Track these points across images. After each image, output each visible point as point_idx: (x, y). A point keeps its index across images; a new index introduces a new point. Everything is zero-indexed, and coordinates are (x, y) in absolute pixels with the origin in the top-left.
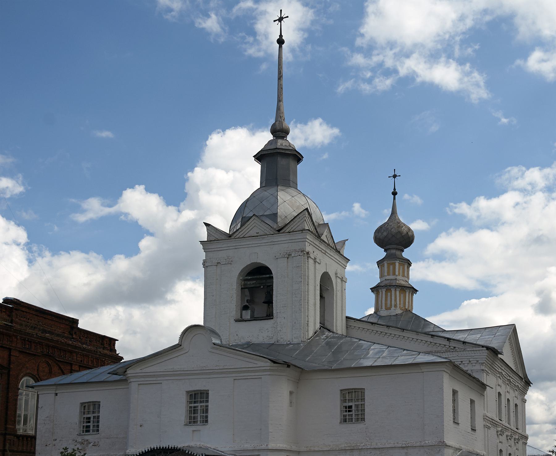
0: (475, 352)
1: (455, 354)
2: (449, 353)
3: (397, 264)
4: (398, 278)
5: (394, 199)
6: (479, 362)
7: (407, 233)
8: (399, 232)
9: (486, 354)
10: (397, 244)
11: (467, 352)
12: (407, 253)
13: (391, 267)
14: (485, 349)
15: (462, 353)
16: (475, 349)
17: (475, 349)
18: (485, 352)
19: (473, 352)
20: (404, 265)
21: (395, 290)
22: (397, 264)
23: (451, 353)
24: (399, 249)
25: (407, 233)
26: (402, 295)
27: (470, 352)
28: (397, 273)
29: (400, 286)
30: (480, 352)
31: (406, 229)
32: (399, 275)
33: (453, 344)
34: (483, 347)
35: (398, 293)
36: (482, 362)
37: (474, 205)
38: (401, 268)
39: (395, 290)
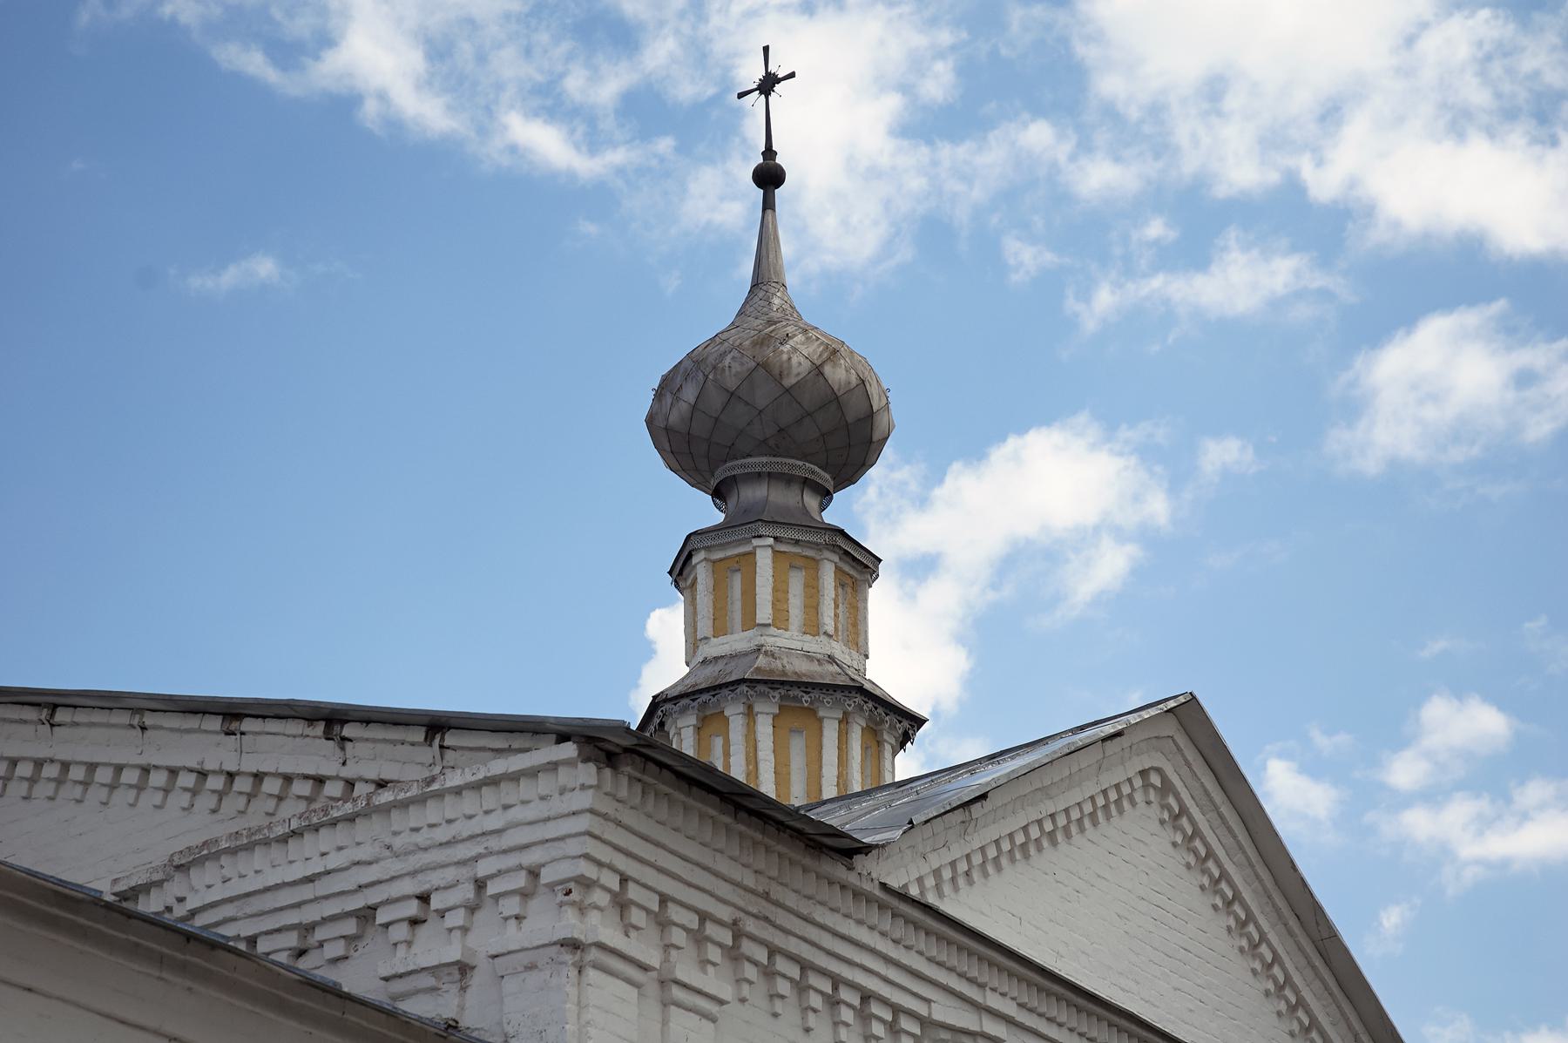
0: (508, 793)
1: (366, 838)
2: (326, 839)
3: (764, 560)
4: (778, 640)
5: (768, 204)
6: (547, 876)
7: (818, 370)
8: (764, 366)
9: (584, 800)
10: (764, 447)
11: (450, 807)
12: (859, 509)
13: (737, 582)
14: (569, 750)
15: (415, 817)
16: (499, 766)
17: (499, 766)
18: (579, 784)
19: (489, 797)
20: (813, 565)
21: (750, 714)
22: (764, 560)
23: (341, 835)
24: (808, 484)
25: (818, 370)
26: (797, 746)
27: (469, 803)
28: (764, 613)
29: (773, 684)
30: (545, 784)
31: (812, 350)
32: (780, 619)
33: (370, 758)
34: (562, 738)
35: (764, 728)
36: (565, 870)
37: (1274, 177)
38: (796, 583)
39: (750, 714)
